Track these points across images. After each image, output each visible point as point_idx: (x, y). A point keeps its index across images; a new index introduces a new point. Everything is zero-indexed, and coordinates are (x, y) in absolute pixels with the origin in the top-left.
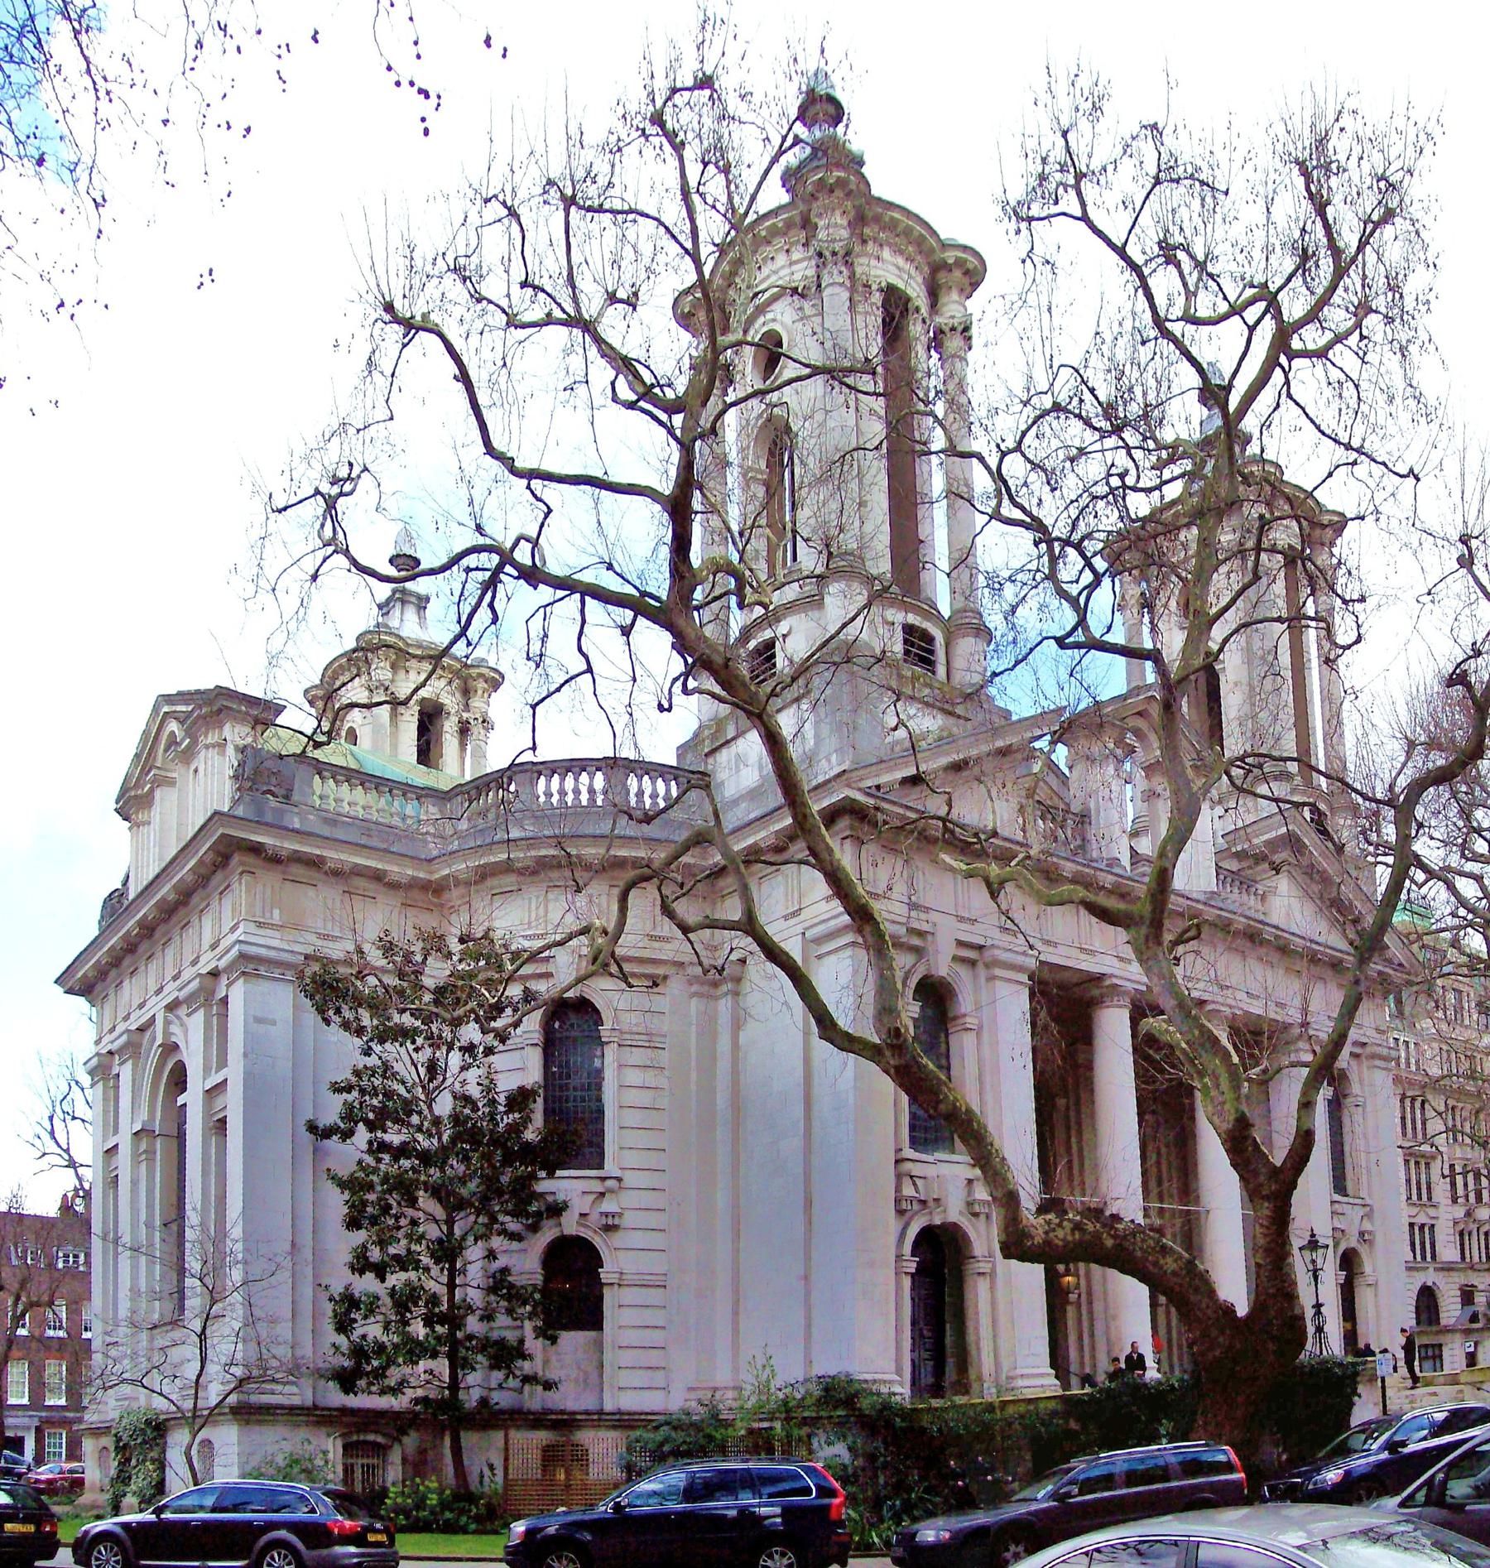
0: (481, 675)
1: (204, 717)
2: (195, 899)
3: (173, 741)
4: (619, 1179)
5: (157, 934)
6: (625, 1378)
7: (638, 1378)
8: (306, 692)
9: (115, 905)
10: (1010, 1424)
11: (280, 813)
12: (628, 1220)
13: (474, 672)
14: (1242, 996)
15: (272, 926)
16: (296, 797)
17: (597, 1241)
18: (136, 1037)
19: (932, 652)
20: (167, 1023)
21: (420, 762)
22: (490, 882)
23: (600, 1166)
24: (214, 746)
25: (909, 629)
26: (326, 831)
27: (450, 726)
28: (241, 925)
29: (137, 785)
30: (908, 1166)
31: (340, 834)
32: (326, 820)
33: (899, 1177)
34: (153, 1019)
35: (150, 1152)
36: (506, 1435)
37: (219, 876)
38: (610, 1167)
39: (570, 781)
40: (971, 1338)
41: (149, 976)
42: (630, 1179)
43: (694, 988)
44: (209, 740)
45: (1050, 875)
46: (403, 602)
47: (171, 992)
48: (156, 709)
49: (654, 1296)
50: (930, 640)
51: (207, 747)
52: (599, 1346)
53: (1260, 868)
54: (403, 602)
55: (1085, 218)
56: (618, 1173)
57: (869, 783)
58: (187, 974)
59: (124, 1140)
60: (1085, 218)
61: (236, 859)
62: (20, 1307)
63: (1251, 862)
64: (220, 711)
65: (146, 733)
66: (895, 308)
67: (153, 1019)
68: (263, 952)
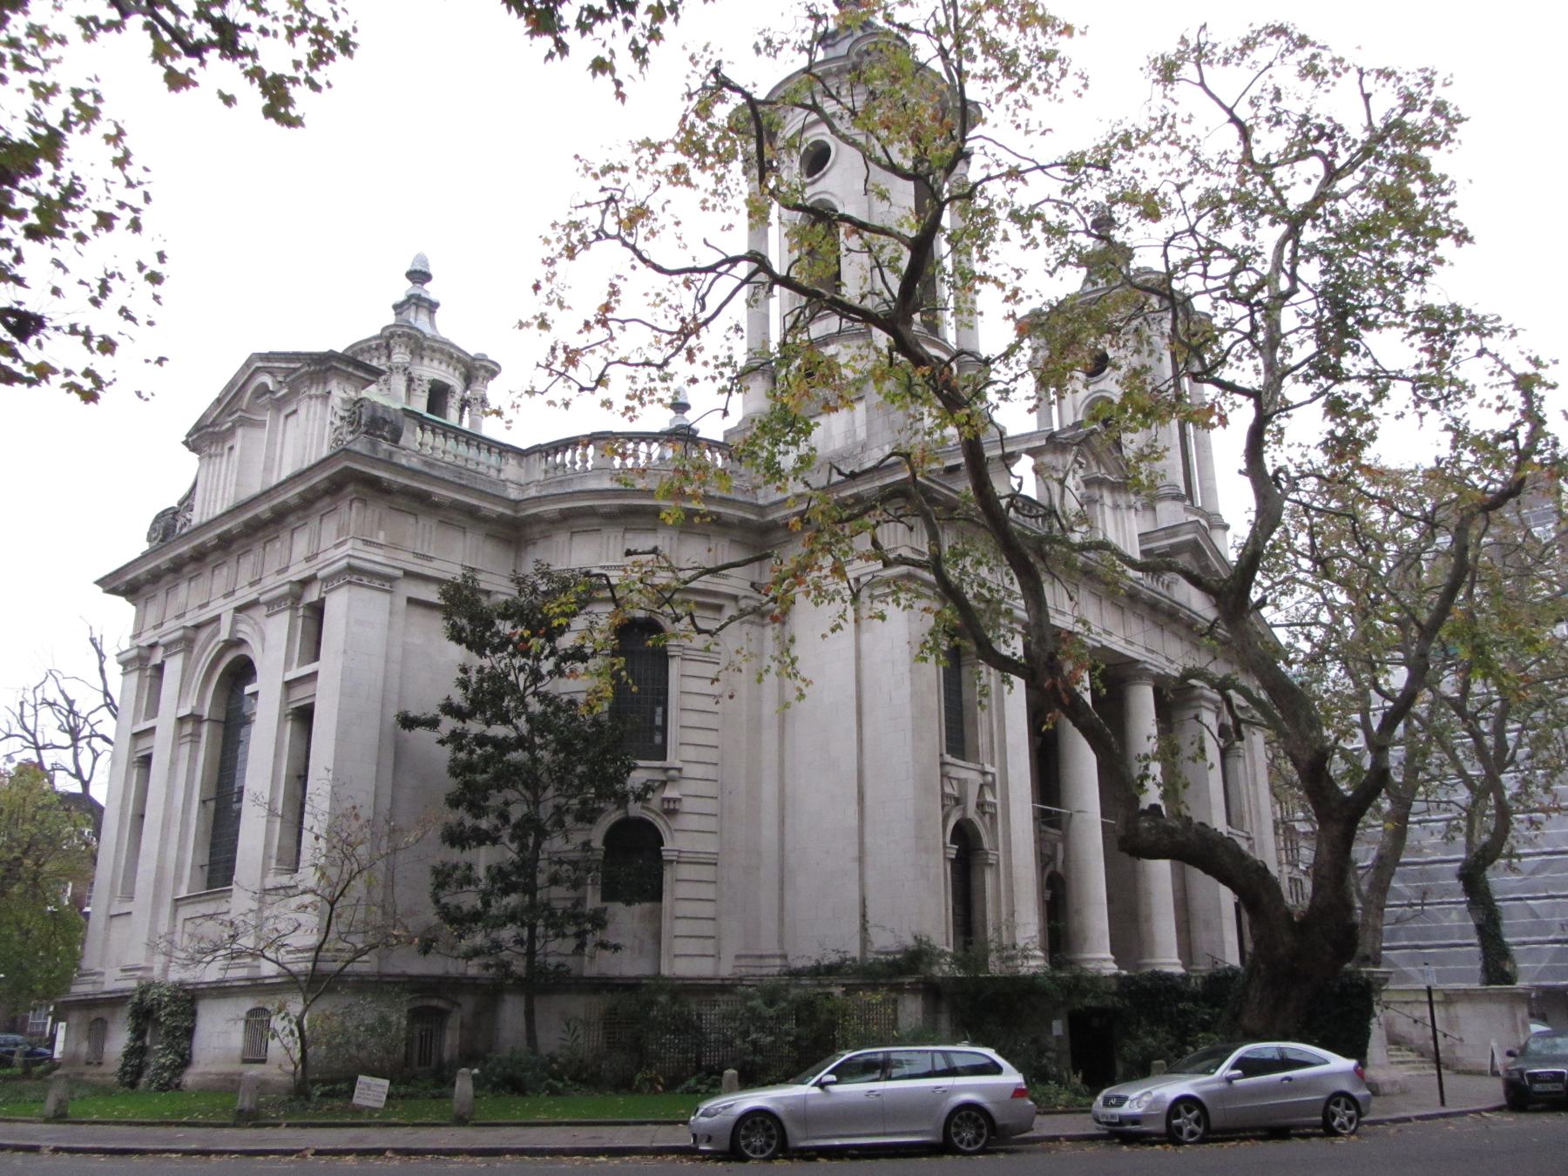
1: (312, 373)
2: (291, 519)
3: (263, 390)
4: (680, 770)
5: (234, 547)
6: (680, 946)
7: (692, 946)
9: (166, 526)
11: (391, 454)
12: (687, 805)
13: (477, 364)
15: (380, 546)
16: (402, 442)
17: (660, 823)
20: (235, 622)
23: (664, 758)
24: (317, 397)
26: (426, 470)
28: (349, 544)
29: (213, 424)
30: (948, 768)
31: (435, 473)
32: (426, 463)
34: (217, 618)
35: (195, 736)
36: (865, 940)
37: (327, 500)
38: (672, 760)
39: (569, 454)
40: (977, 916)
41: (220, 580)
42: (689, 770)
44: (313, 391)
46: (418, 306)
47: (245, 595)
48: (248, 364)
49: (706, 872)
51: (310, 397)
52: (657, 917)
54: (418, 306)
55: (1202, 84)
56: (678, 764)
58: (269, 582)
59: (165, 723)
60: (1202, 84)
61: (351, 488)
62: (1238, 699)
64: (328, 370)
65: (232, 384)
67: (217, 618)
68: (368, 566)
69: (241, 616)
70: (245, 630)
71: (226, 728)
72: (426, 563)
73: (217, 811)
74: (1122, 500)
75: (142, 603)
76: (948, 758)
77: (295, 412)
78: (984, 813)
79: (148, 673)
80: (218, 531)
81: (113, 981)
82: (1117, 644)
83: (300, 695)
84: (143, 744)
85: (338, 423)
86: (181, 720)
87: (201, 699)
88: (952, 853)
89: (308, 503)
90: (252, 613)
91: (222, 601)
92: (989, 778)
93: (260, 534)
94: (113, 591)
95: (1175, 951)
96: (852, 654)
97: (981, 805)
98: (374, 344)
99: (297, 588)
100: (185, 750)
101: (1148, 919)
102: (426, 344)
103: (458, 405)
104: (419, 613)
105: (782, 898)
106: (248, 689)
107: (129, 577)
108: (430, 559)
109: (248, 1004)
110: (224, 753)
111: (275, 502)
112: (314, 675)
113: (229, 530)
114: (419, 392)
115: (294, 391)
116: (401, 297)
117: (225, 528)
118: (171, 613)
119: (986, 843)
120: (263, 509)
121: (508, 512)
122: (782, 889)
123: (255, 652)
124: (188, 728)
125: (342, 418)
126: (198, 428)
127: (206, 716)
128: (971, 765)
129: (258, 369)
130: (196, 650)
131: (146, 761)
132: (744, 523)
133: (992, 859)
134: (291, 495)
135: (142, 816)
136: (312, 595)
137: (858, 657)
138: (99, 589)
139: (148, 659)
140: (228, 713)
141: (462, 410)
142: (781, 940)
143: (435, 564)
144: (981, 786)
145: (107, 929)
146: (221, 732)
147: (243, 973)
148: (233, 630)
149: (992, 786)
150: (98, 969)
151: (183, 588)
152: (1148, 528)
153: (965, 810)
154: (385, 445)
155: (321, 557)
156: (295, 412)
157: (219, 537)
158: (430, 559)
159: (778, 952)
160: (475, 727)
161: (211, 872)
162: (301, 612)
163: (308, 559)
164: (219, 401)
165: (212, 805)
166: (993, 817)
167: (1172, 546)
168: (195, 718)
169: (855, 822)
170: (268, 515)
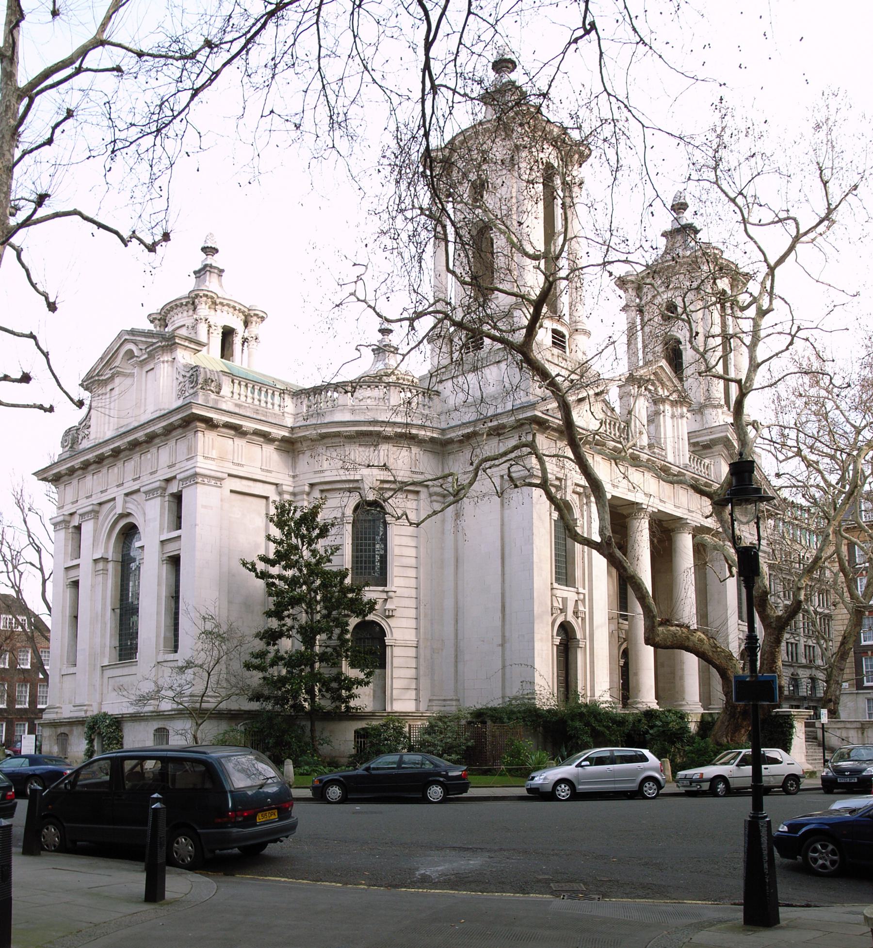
0: (255, 315)
1: (163, 347)
2: (157, 441)
3: (130, 354)
5: (121, 456)
8: (150, 315)
10: (640, 721)
11: (216, 401)
13: (252, 313)
14: (657, 501)
15: (213, 459)
17: (384, 624)
18: (97, 508)
19: (564, 342)
20: (125, 502)
21: (222, 357)
22: (325, 441)
23: (386, 586)
25: (554, 331)
26: (237, 410)
27: (237, 341)
31: (242, 412)
33: (552, 595)
34: (114, 499)
37: (179, 431)
43: (434, 498)
45: (801, 509)
48: (119, 336)
50: (563, 336)
53: (489, 377)
56: (394, 589)
57: (545, 408)
63: (700, 448)
66: (549, 173)
69: (128, 499)
70: (132, 508)
71: (122, 566)
72: (239, 468)
73: (121, 615)
74: (679, 410)
75: (62, 487)
76: (556, 585)
77: (153, 369)
78: (578, 618)
79: (70, 530)
80: (112, 447)
81: (67, 712)
82: (669, 508)
83: (171, 549)
84: (73, 573)
85: (181, 379)
86: (96, 561)
87: (106, 548)
88: (557, 641)
89: (169, 431)
90: (134, 496)
91: (116, 489)
92: (581, 596)
93: (137, 449)
94: (45, 479)
95: (697, 698)
96: (499, 523)
97: (576, 613)
98: (184, 301)
99: (163, 484)
100: (100, 578)
101: (682, 678)
102: (218, 301)
103: (241, 341)
104: (234, 495)
105: (456, 667)
106: (137, 544)
107: (55, 471)
108: (242, 465)
109: (156, 725)
110: (122, 580)
111: (148, 431)
112: (179, 537)
113: (119, 446)
114: (215, 333)
115: (151, 356)
116: (198, 267)
117: (116, 445)
118: (82, 494)
119: (579, 635)
120: (140, 435)
121: (287, 434)
122: (456, 662)
123: (138, 520)
124: (101, 565)
125: (184, 376)
126: (89, 376)
127: (110, 559)
128: (572, 589)
129: (126, 340)
130: (101, 518)
131: (76, 584)
132: (432, 439)
133: (581, 644)
134: (158, 427)
135: (76, 617)
136: (173, 488)
137: (502, 525)
138: (35, 478)
139: (69, 522)
140: (123, 556)
141: (243, 345)
142: (456, 691)
143: (245, 468)
144: (576, 601)
145: (61, 682)
146: (120, 568)
147: (151, 708)
148: (124, 508)
149: (583, 601)
150: (58, 705)
151: (89, 478)
152: (696, 427)
153: (566, 615)
154: (213, 396)
155: (177, 466)
156: (153, 369)
157: (112, 450)
158: (242, 465)
159: (454, 698)
160: (275, 570)
161: (121, 650)
162: (167, 498)
163: (170, 467)
164: (102, 359)
165: (118, 611)
166: (583, 619)
167: (711, 440)
168: (104, 559)
169: (499, 623)
170: (143, 438)
